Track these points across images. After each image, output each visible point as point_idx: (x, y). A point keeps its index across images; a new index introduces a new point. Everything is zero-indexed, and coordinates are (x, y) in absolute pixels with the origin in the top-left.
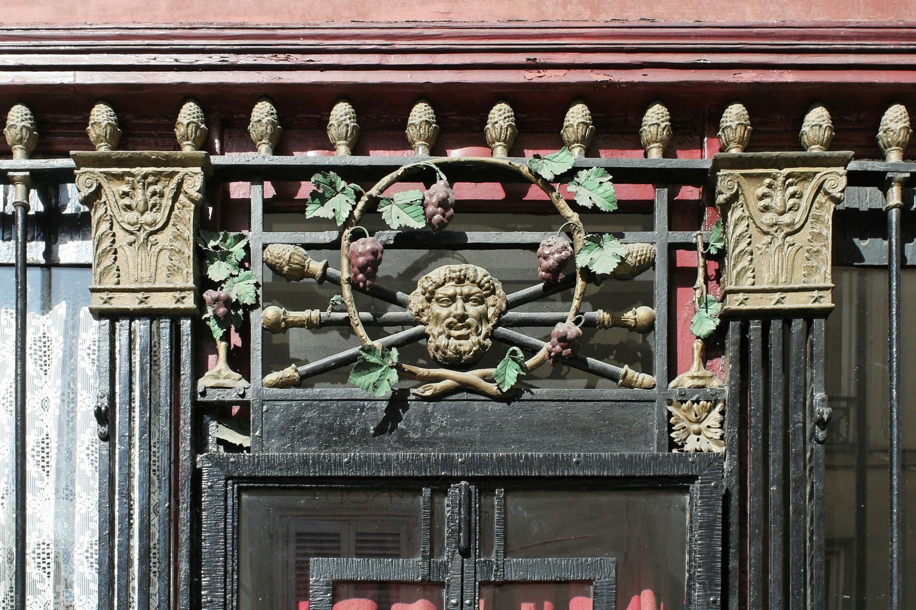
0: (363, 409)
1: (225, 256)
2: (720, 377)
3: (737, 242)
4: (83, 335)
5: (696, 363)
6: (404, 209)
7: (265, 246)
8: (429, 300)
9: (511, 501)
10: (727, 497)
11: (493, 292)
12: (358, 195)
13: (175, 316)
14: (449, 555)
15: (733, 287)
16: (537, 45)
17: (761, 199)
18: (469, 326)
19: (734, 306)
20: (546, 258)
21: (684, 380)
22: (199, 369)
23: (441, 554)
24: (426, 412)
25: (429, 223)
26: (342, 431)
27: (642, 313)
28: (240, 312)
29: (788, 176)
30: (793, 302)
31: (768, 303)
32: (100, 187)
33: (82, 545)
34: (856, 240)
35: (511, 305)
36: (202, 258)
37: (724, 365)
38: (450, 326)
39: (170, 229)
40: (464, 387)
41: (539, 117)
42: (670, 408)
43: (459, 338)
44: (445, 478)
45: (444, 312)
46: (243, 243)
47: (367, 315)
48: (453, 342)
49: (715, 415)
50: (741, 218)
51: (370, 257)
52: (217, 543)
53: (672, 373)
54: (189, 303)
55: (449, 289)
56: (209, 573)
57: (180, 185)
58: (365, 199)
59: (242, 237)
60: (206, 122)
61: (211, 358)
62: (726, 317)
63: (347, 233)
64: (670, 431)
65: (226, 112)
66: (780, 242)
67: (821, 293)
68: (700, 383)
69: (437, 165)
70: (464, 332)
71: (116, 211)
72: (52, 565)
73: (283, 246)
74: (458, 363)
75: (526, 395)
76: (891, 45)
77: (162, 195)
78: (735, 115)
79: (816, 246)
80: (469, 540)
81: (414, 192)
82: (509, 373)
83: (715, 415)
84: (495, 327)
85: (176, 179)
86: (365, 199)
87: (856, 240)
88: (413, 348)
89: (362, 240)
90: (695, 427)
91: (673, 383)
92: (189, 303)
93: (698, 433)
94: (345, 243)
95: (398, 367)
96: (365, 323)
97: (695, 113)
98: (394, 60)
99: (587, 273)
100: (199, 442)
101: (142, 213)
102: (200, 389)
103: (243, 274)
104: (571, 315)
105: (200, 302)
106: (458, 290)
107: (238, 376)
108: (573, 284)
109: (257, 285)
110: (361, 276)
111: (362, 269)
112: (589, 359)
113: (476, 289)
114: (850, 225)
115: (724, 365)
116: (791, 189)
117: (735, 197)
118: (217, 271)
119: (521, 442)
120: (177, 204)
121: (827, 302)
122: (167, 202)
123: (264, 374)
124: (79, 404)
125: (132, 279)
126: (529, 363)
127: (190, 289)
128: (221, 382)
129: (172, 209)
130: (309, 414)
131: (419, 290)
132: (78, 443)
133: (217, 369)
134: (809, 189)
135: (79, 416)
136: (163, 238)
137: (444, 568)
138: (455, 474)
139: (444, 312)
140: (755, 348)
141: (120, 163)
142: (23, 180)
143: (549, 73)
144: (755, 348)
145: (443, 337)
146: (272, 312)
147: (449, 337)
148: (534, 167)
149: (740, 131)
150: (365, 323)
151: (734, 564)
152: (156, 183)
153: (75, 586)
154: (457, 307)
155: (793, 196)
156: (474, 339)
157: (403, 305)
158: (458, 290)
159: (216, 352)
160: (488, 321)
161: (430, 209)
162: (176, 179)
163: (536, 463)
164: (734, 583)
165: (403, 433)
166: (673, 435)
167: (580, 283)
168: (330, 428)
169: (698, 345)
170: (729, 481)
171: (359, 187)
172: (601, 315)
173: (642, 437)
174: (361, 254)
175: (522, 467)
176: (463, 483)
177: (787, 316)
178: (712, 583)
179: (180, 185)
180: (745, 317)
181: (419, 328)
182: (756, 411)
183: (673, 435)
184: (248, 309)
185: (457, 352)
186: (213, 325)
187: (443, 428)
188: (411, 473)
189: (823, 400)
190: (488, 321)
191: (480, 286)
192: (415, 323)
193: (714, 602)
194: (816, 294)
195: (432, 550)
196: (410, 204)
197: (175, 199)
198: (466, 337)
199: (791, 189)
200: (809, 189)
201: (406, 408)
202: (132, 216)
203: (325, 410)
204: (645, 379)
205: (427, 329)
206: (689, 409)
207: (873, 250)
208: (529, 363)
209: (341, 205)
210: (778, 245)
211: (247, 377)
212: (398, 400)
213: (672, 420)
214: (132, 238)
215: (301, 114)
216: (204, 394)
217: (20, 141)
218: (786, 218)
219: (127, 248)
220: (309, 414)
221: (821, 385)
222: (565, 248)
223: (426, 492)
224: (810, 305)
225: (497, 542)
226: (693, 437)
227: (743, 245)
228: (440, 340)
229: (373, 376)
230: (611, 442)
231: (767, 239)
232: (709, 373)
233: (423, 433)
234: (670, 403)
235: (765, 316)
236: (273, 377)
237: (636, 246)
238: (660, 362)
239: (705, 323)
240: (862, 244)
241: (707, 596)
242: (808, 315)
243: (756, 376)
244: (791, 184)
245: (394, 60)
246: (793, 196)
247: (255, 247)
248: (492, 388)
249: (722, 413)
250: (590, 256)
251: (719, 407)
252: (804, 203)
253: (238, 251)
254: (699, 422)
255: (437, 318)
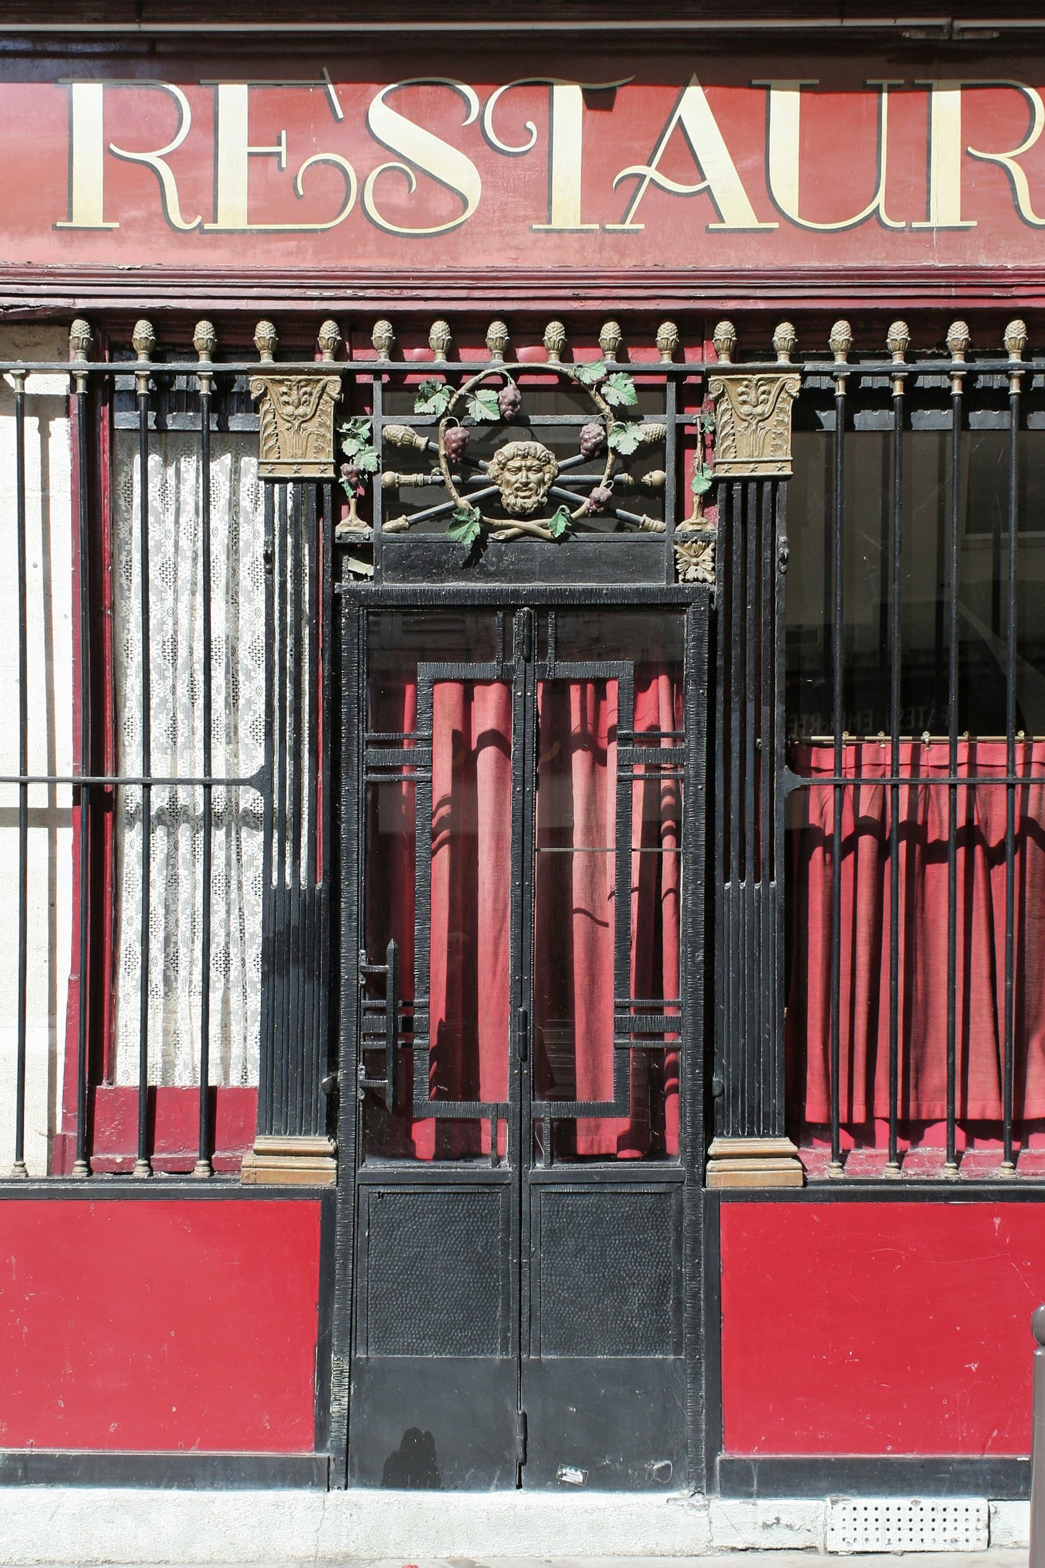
0: (454, 548)
1: (355, 436)
2: (711, 523)
3: (723, 427)
4: (243, 480)
5: (695, 513)
6: (483, 407)
7: (383, 426)
8: (502, 469)
9: (560, 622)
10: (713, 615)
11: (549, 463)
12: (452, 393)
13: (319, 482)
14: (515, 660)
15: (720, 460)
16: (582, 282)
17: (740, 395)
18: (531, 490)
19: (722, 474)
20: (586, 441)
21: (686, 526)
22: (337, 519)
23: (510, 659)
24: (500, 550)
25: (502, 416)
26: (440, 565)
27: (655, 476)
28: (366, 476)
29: (759, 380)
30: (762, 471)
31: (745, 472)
32: (266, 388)
33: (246, 643)
34: (817, 412)
35: (561, 470)
36: (339, 438)
37: (715, 510)
38: (517, 489)
39: (317, 419)
40: (527, 533)
41: (582, 329)
42: (676, 547)
43: (524, 498)
44: (513, 605)
45: (513, 478)
46: (368, 426)
47: (456, 477)
48: (520, 501)
49: (709, 551)
50: (726, 410)
51: (461, 443)
52: (352, 653)
53: (679, 518)
54: (330, 474)
55: (516, 463)
56: (347, 674)
57: (324, 388)
58: (456, 396)
59: (367, 421)
60: (340, 334)
61: (344, 508)
62: (716, 481)
63: (444, 421)
64: (676, 564)
65: (356, 327)
66: (754, 427)
67: (784, 464)
68: (698, 528)
69: (507, 370)
70: (527, 493)
71: (278, 406)
72: (223, 657)
73: (397, 430)
74: (523, 515)
75: (572, 538)
76: (834, 282)
77: (311, 394)
78: (724, 330)
79: (780, 429)
80: (530, 650)
81: (490, 395)
82: (559, 524)
83: (709, 551)
84: (550, 487)
85: (321, 384)
86: (456, 396)
87: (817, 412)
88: (492, 505)
89: (454, 429)
90: (695, 560)
91: (679, 528)
92: (330, 474)
93: (697, 564)
94: (442, 428)
95: (481, 521)
96: (455, 484)
97: (695, 327)
98: (477, 294)
99: (614, 450)
100: (337, 574)
101: (297, 408)
102: (337, 534)
103: (368, 448)
104: (604, 478)
105: (338, 472)
106: (523, 463)
107: (365, 523)
108: (607, 456)
109: (378, 457)
110: (453, 456)
111: (455, 451)
112: (618, 511)
113: (536, 462)
114: (807, 407)
115: (715, 510)
116: (762, 389)
117: (722, 395)
118: (349, 447)
119: (568, 572)
120: (322, 401)
121: (788, 471)
122: (314, 399)
123: (384, 522)
124: (241, 534)
125: (289, 455)
126: (574, 515)
127: (331, 463)
128: (352, 528)
129: (318, 404)
130: (417, 553)
131: (495, 460)
132: (241, 565)
133: (349, 518)
134: (775, 388)
135: (241, 543)
136: (311, 426)
137: (512, 669)
138: (520, 603)
139: (513, 478)
140: (737, 503)
141: (282, 372)
142: (209, 378)
143: (589, 302)
144: (737, 503)
145: (512, 497)
146: (388, 477)
147: (516, 497)
148: (578, 374)
149: (727, 344)
150: (455, 484)
151: (720, 662)
152: (306, 386)
153: (240, 673)
154: (522, 477)
155: (763, 393)
156: (534, 499)
157: (484, 470)
158: (523, 463)
159: (348, 504)
160: (545, 484)
161: (503, 407)
162: (321, 384)
163: (577, 594)
164: (720, 677)
165: (483, 566)
166: (678, 567)
167: (611, 457)
168: (431, 562)
169: (696, 499)
170: (718, 604)
171: (452, 388)
172: (625, 477)
173: (656, 569)
174: (454, 442)
175: (567, 597)
176: (526, 609)
177: (760, 480)
178: (701, 680)
179: (324, 388)
180: (730, 481)
181: (495, 487)
182: (737, 550)
183: (678, 567)
184: (371, 474)
185: (522, 508)
186: (346, 486)
187: (512, 563)
188: (489, 602)
189: (784, 543)
190: (545, 484)
191: (539, 459)
192: (493, 484)
193: (703, 694)
194: (779, 465)
195: (504, 655)
196: (490, 402)
197: (320, 398)
198: (529, 497)
199: (762, 389)
200: (775, 388)
201: (485, 547)
202: (289, 409)
203: (427, 549)
204: (658, 524)
205: (501, 489)
206: (690, 547)
207: (828, 419)
208: (574, 515)
209: (439, 402)
210: (753, 433)
211: (371, 524)
212: (480, 542)
213: (677, 556)
214: (289, 425)
215: (410, 328)
216: (340, 538)
217: (206, 349)
218: (759, 409)
219: (286, 433)
220: (417, 553)
221: (784, 531)
222: (599, 434)
223: (500, 615)
224: (776, 473)
225: (551, 651)
226: (693, 568)
227: (727, 429)
228: (510, 499)
229: (463, 529)
230: (633, 572)
231: (745, 424)
232: (704, 520)
233: (498, 567)
234: (676, 543)
235: (745, 481)
236: (389, 525)
237: (651, 428)
238: (670, 513)
239: (699, 485)
240: (822, 415)
241: (697, 690)
242: (775, 480)
243: (737, 525)
244: (762, 385)
245: (477, 294)
246: (763, 393)
247: (377, 428)
248: (547, 533)
249: (713, 550)
250: (618, 439)
251: (712, 545)
252: (772, 398)
253: (364, 431)
254: (697, 556)
255: (508, 483)
